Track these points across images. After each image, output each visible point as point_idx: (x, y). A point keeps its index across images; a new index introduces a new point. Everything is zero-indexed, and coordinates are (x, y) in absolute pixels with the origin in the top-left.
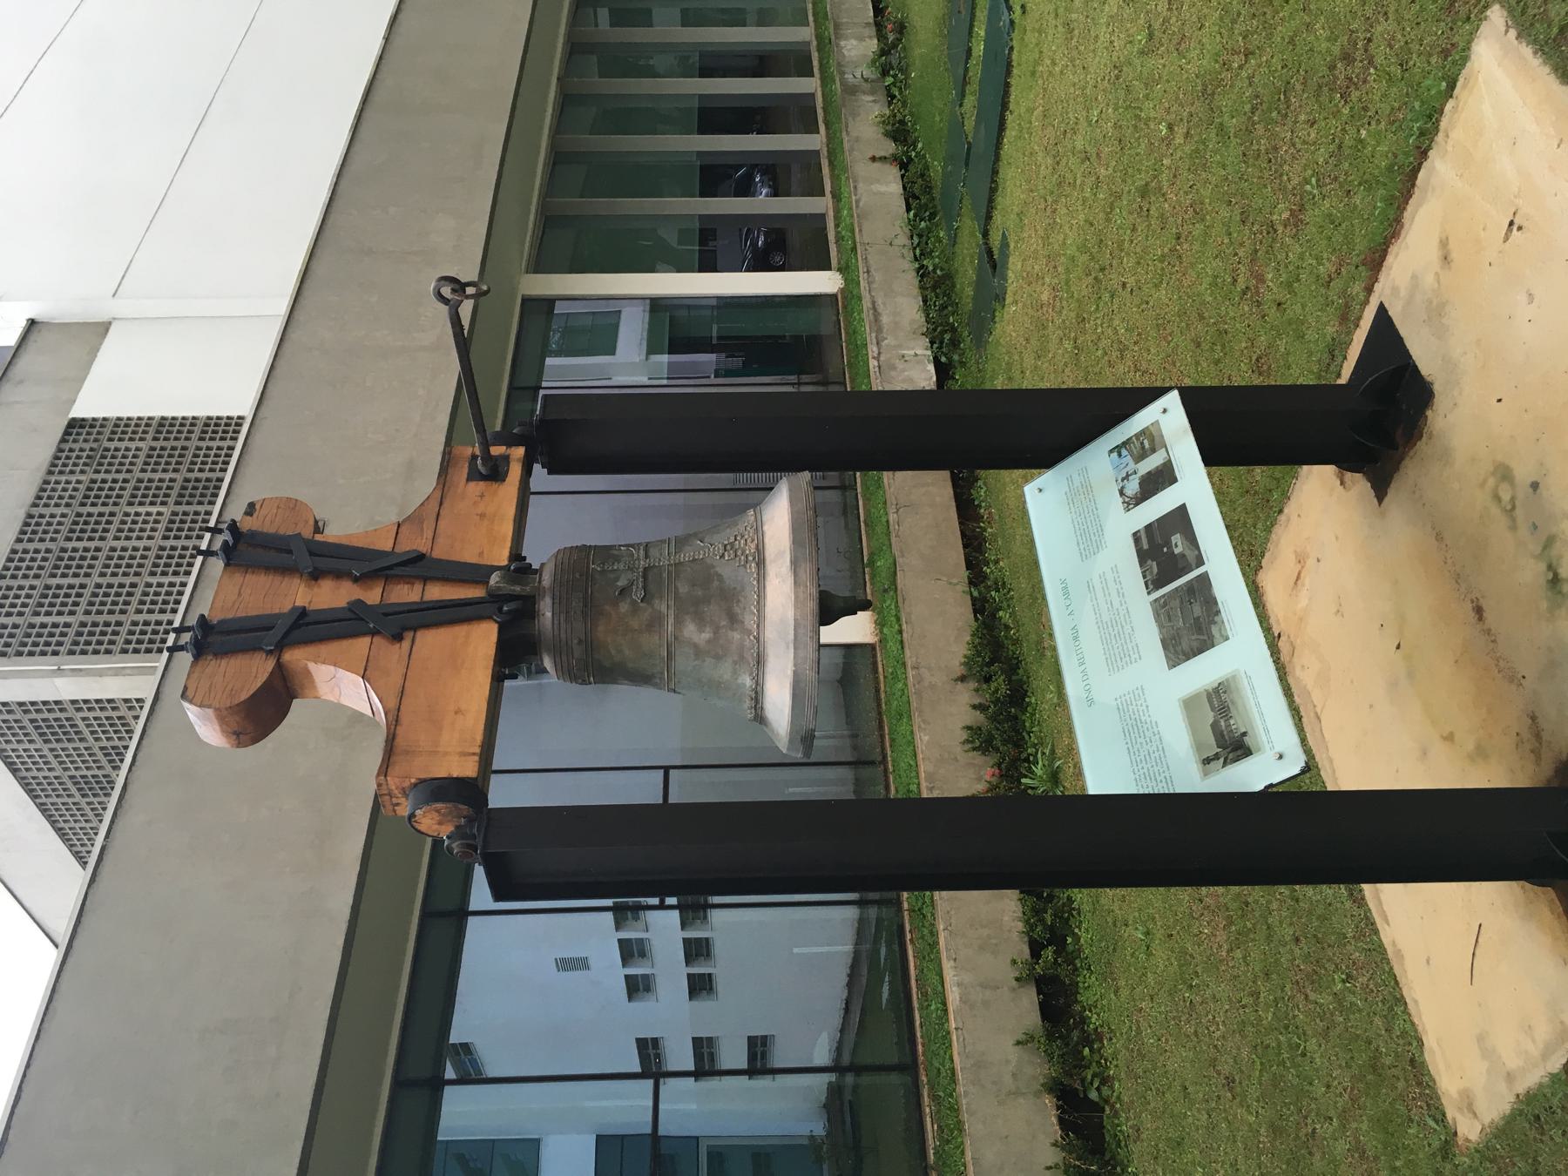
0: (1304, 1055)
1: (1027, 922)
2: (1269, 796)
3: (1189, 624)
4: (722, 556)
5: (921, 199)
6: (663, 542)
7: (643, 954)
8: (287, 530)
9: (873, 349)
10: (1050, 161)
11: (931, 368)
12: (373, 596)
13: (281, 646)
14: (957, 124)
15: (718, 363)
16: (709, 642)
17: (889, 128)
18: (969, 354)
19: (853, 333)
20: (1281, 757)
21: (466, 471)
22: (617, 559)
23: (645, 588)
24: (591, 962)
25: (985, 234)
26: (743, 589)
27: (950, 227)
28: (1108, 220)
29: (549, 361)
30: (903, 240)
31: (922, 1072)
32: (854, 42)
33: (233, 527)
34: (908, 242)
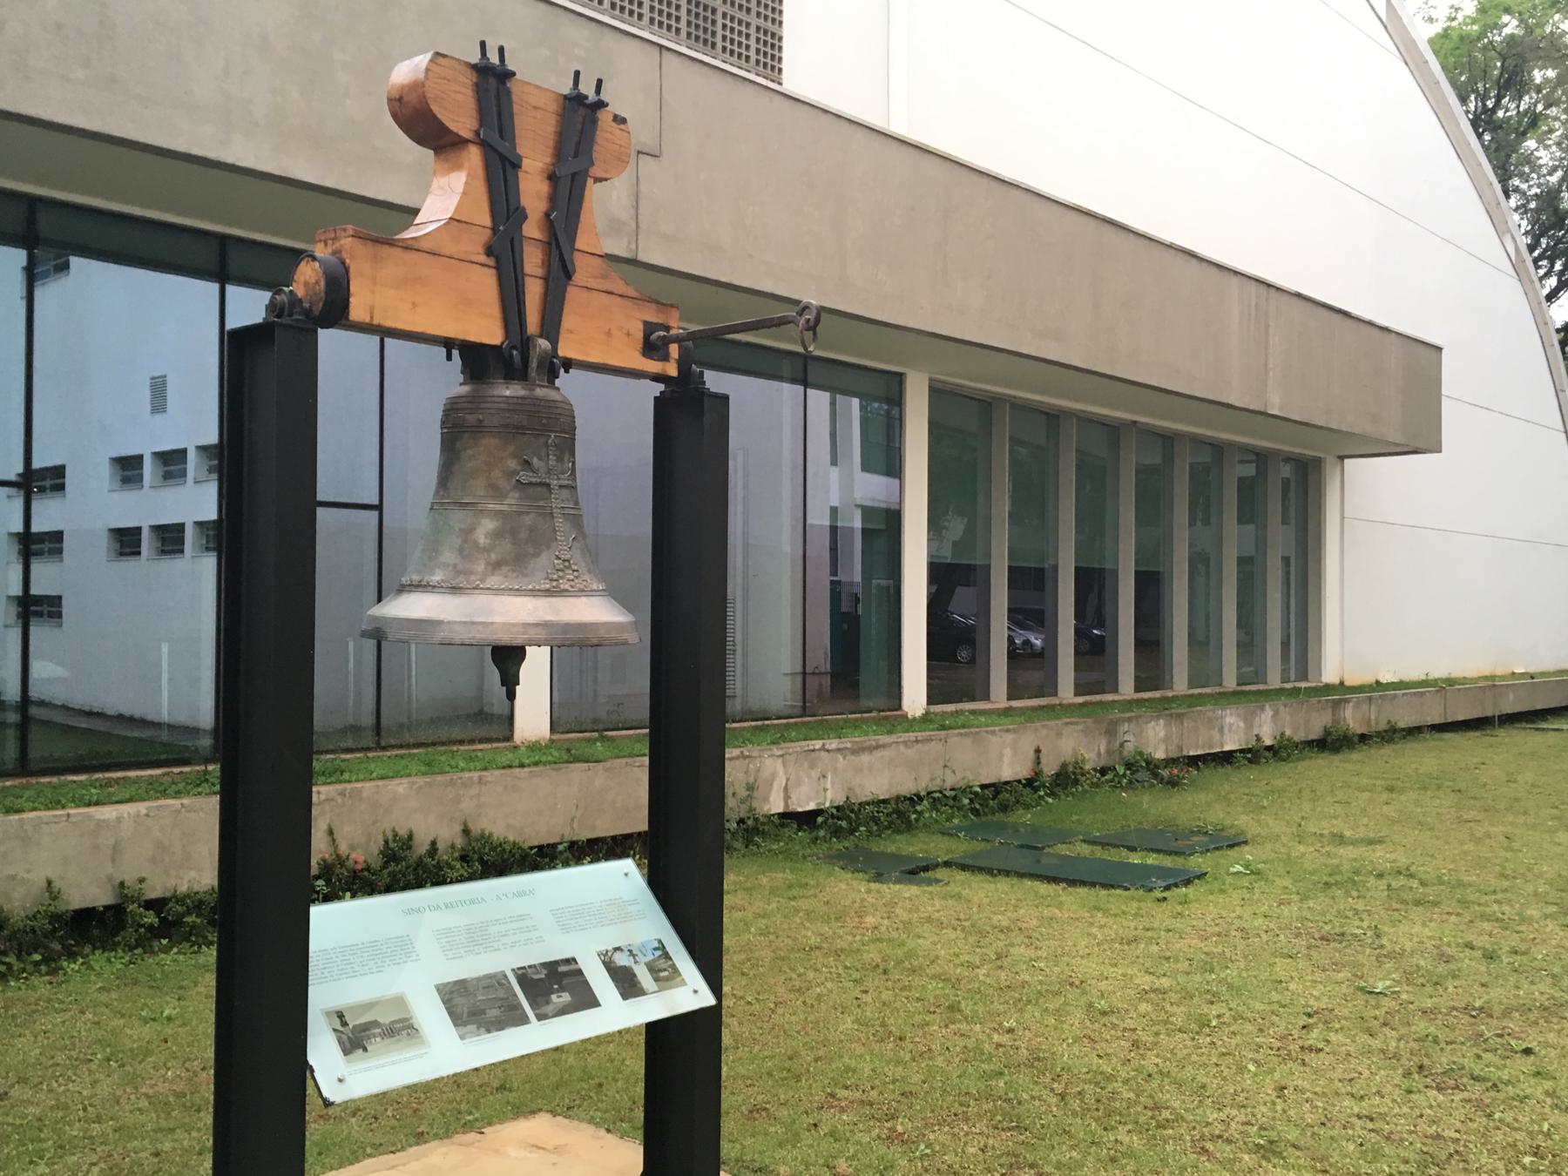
0: (31, 1162)
1: (187, 896)
2: (302, 1070)
3: (475, 1005)
4: (558, 558)
5: (992, 801)
6: (577, 503)
7: (167, 476)
8: (599, 153)
9: (833, 744)
10: (1005, 923)
11: (812, 806)
12: (532, 229)
13: (484, 145)
14: (1065, 837)
15: (852, 584)
16: (476, 542)
17: (1071, 769)
18: (825, 846)
19: (856, 725)
20: (340, 1080)
21: (654, 320)
22: (560, 459)
23: (531, 484)
24: (158, 417)
25: (947, 864)
26: (525, 575)
27: (960, 829)
28: (934, 977)
29: (856, 402)
30: (951, 780)
31: (17, 782)
32: (1162, 734)
33: (601, 105)
34: (948, 785)
